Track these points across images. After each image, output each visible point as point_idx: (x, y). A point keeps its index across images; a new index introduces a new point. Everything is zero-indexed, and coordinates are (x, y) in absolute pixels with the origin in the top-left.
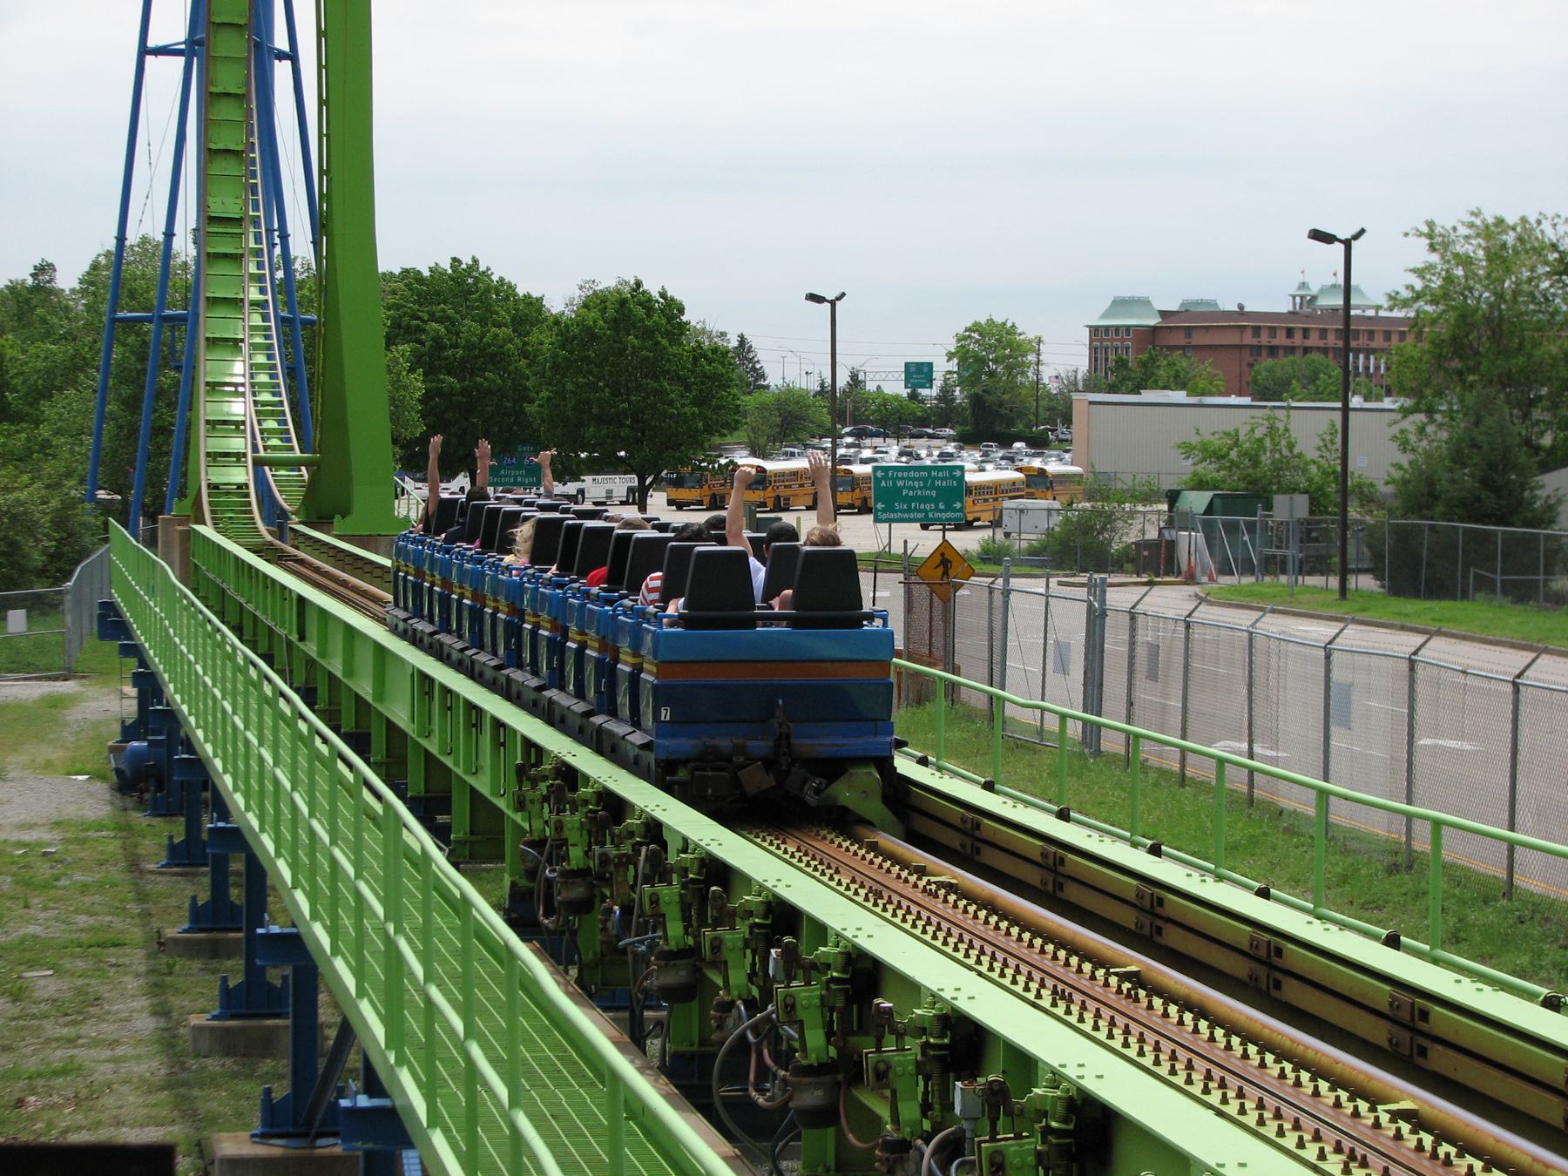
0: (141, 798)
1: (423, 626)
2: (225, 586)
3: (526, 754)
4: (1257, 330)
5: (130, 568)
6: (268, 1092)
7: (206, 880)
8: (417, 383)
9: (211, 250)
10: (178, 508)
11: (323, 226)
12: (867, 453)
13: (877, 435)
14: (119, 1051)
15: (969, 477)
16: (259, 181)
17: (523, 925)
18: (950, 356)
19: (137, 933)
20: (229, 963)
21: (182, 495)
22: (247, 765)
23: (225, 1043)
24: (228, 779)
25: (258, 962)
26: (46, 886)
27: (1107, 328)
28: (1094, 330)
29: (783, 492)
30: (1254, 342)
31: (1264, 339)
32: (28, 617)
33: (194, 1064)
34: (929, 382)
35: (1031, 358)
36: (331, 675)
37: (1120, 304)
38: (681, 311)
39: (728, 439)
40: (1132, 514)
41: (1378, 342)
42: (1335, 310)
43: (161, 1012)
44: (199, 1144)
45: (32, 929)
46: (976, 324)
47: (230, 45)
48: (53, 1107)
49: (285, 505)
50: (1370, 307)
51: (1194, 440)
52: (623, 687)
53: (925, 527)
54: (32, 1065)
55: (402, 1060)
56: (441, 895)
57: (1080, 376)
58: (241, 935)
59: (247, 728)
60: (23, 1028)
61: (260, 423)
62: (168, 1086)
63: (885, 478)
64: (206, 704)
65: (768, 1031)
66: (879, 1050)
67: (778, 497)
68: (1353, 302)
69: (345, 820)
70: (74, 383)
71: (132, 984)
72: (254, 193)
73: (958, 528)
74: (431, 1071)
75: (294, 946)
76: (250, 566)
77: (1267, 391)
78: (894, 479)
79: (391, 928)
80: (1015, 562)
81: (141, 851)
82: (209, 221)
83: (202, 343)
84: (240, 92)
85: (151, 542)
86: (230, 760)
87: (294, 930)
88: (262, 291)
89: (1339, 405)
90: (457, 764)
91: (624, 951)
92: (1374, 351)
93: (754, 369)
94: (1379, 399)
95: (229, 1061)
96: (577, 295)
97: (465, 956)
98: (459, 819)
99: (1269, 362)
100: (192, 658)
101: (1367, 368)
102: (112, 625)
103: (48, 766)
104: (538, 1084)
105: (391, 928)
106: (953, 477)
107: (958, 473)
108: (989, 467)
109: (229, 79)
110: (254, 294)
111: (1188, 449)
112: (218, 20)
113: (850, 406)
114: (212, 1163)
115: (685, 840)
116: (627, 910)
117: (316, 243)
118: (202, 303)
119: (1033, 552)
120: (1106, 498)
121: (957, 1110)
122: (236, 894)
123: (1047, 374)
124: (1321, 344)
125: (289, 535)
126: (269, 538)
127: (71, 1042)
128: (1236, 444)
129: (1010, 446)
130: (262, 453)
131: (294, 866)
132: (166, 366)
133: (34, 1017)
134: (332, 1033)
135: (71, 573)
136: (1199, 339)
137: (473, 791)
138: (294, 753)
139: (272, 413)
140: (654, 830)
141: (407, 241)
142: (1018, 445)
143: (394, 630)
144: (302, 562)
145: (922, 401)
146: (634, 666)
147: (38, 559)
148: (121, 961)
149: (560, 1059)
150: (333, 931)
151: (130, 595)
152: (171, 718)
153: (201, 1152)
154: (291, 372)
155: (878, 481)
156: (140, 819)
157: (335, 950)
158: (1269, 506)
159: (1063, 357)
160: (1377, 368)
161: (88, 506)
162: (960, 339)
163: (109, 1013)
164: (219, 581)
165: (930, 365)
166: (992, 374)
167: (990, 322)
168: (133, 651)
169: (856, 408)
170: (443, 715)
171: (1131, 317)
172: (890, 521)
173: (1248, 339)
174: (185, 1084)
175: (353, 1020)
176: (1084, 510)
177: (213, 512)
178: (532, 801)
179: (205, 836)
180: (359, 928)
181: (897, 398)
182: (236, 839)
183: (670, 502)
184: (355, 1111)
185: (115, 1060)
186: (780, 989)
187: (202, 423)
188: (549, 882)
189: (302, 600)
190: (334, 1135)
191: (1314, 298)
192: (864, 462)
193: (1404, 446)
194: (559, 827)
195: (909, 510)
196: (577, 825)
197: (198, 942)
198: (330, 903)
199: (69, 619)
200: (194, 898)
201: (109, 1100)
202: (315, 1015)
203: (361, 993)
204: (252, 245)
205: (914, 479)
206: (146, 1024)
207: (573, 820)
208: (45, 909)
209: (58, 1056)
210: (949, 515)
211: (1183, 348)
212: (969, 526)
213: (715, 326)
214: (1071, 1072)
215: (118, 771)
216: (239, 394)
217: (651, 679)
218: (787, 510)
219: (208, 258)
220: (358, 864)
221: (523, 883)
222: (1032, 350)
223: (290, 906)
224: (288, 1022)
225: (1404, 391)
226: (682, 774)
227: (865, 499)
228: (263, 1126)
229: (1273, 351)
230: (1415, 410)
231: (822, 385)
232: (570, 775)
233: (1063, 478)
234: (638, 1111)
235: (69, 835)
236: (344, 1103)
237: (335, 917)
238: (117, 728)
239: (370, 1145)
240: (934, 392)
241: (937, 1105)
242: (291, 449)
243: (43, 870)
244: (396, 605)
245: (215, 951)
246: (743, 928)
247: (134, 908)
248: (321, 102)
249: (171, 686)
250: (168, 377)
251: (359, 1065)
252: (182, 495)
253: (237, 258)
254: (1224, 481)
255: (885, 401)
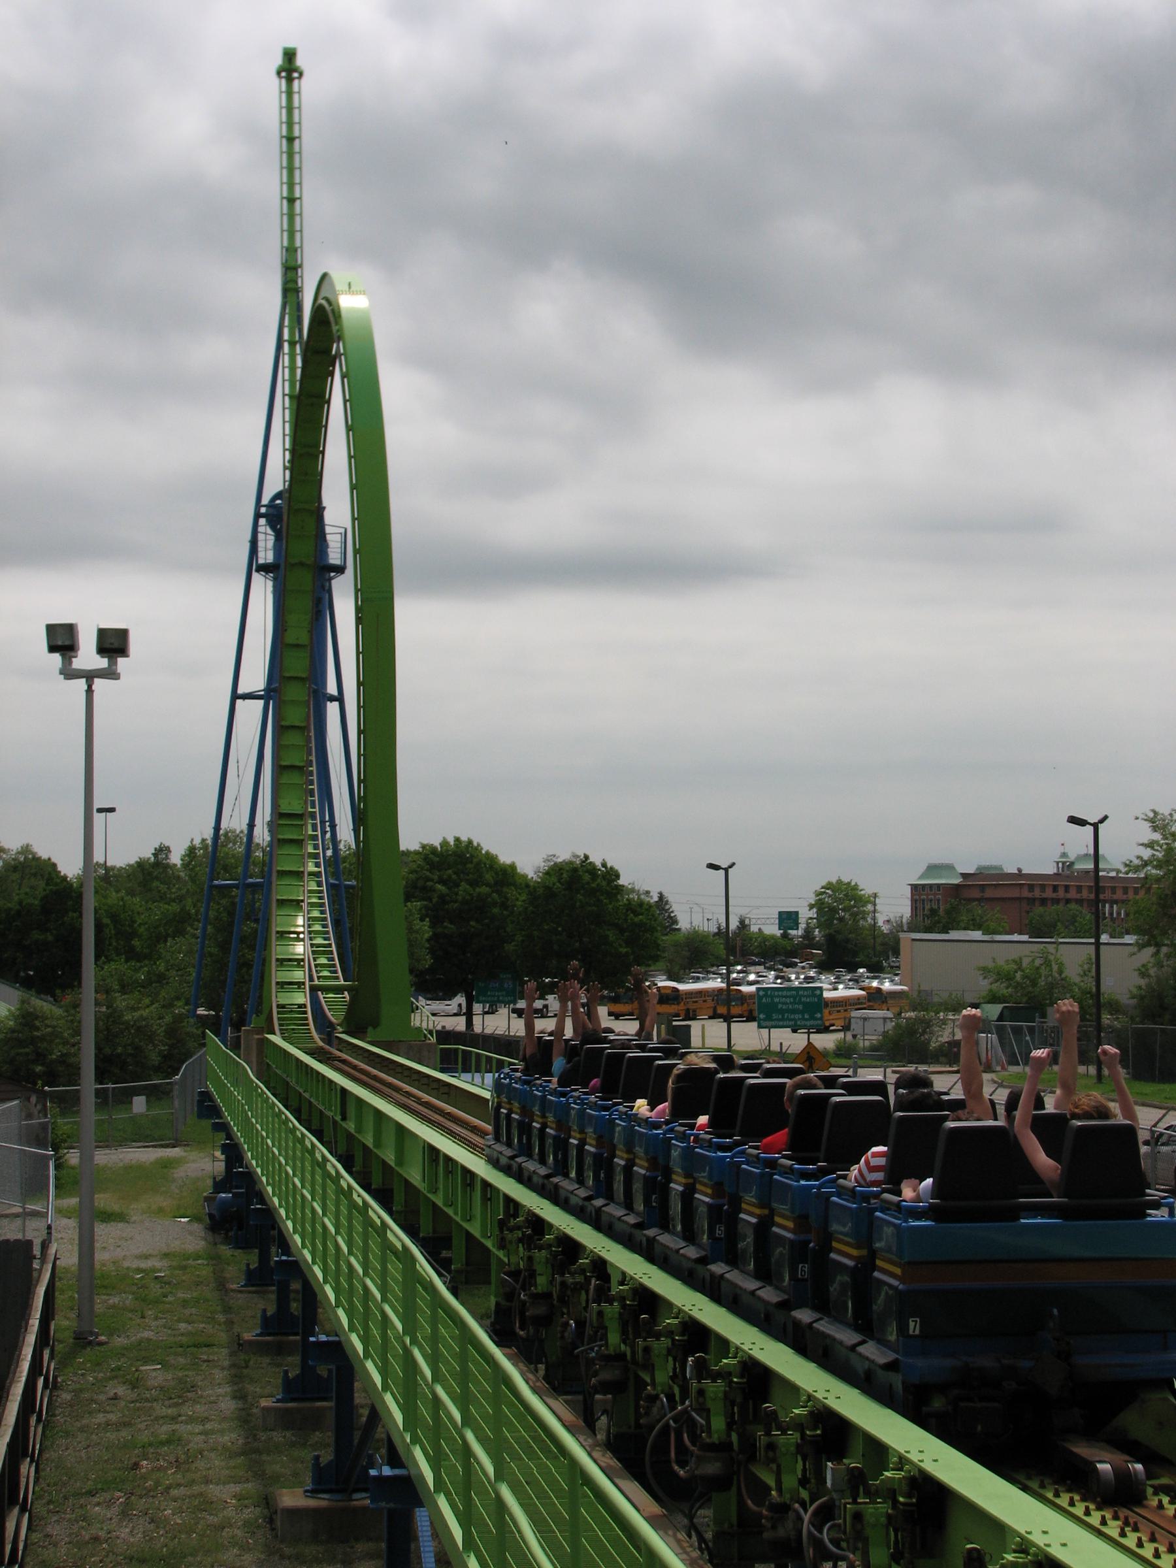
0: (226, 1234)
1: (531, 1166)
2: (288, 1079)
3: (507, 1207)
4: (1031, 887)
5: (222, 1067)
6: (317, 1458)
7: (273, 1297)
8: (425, 929)
9: (281, 837)
10: (255, 1022)
11: (361, 819)
12: (752, 977)
13: (759, 964)
14: (208, 1426)
15: (826, 995)
16: (315, 787)
17: (502, 1337)
18: (811, 907)
19: (223, 1337)
20: (290, 1359)
21: (258, 1012)
22: (303, 1213)
23: (285, 1420)
24: (290, 1224)
25: (310, 1362)
26: (157, 1302)
27: (924, 886)
28: (915, 888)
29: (692, 1006)
30: (1030, 895)
31: (1037, 893)
32: (147, 1102)
33: (263, 1436)
34: (796, 926)
35: (870, 907)
36: (384, 1163)
37: (933, 869)
38: (618, 876)
39: (652, 968)
40: (944, 1022)
41: (1119, 895)
42: (1087, 872)
43: (240, 1396)
44: (266, 1498)
45: (147, 1334)
46: (829, 883)
47: (295, 692)
48: (159, 1469)
49: (333, 1019)
50: (1113, 870)
51: (990, 965)
52: (619, 1178)
53: (794, 1031)
54: (144, 1437)
55: (415, 1440)
56: (444, 1311)
57: (904, 920)
58: (298, 1338)
59: (303, 1186)
60: (138, 1409)
61: (315, 960)
62: (243, 1453)
63: (766, 995)
64: (274, 1167)
65: (684, 1419)
66: (855, 1502)
67: (688, 1010)
68: (1101, 866)
69: (394, 1279)
70: (180, 932)
71: (219, 1375)
72: (312, 796)
73: (818, 1032)
74: (437, 1448)
75: (337, 1351)
76: (307, 1065)
77: (1038, 930)
78: (772, 997)
79: (408, 1340)
80: (861, 1057)
81: (228, 1275)
82: (280, 816)
83: (274, 904)
84: (303, 724)
85: (236, 1046)
86: (291, 1209)
87: (336, 1339)
88: (317, 865)
89: (1093, 940)
90: (456, 1214)
91: (577, 1356)
92: (1116, 902)
93: (669, 917)
94: (1121, 936)
95: (288, 1434)
96: (544, 866)
97: (463, 1358)
98: (457, 1254)
99: (1041, 909)
100: (264, 1134)
101: (1111, 914)
102: (207, 1108)
103: (161, 1210)
104: (516, 1457)
105: (408, 1340)
106: (814, 995)
107: (818, 992)
108: (841, 986)
109: (294, 716)
110: (311, 867)
111: (985, 971)
112: (287, 675)
113: (739, 943)
114: (276, 1512)
115: (624, 1274)
116: (581, 1324)
117: (356, 831)
118: (274, 875)
119: (873, 1048)
120: (926, 1010)
121: (829, 1483)
122: (295, 1307)
123: (881, 920)
124: (1078, 896)
125: (335, 1042)
126: (321, 1044)
127: (174, 1419)
128: (1020, 968)
129: (855, 971)
130: (316, 982)
131: (337, 1290)
132: (248, 919)
133: (147, 1400)
134: (365, 1412)
135: (179, 1069)
136: (989, 894)
137: (468, 1233)
138: (337, 1204)
139: (324, 953)
140: (600, 1266)
141: (420, 825)
142: (861, 970)
143: (494, 1163)
144: (344, 1061)
145: (791, 939)
146: (627, 1160)
147: (154, 1058)
148: (211, 1357)
149: (533, 1438)
150: (365, 1340)
151: (221, 1086)
152: (249, 1178)
153: (268, 1503)
154: (337, 923)
155: (760, 998)
156: (225, 1250)
157: (367, 1355)
158: (1044, 1015)
159: (892, 907)
160: (1119, 914)
161: (192, 1020)
162: (818, 894)
163: (202, 1397)
164: (284, 1076)
165: (797, 913)
166: (841, 919)
167: (839, 882)
168: (223, 1127)
169: (743, 945)
170: (464, 1192)
171: (941, 877)
172: (770, 1028)
173: (1026, 894)
174: (257, 1451)
175: (379, 1407)
176: (910, 1018)
177: (280, 1025)
178: (511, 1242)
179: (272, 1263)
180: (384, 1336)
181: (773, 937)
182: (296, 1269)
183: (610, 1014)
184: (380, 1479)
185: (205, 1433)
186: (694, 1384)
187: (274, 960)
188: (524, 1303)
189: (344, 1091)
190: (365, 1490)
191: (1072, 863)
192: (751, 983)
193: (1143, 973)
194: (530, 1259)
195: (783, 1019)
196: (543, 1260)
197: (267, 1343)
198: (364, 1316)
199: (176, 1103)
200: (264, 1311)
201: (200, 1464)
202: (352, 1398)
203: (386, 1387)
204: (310, 832)
205: (786, 997)
206: (228, 1405)
207: (541, 1256)
208: (156, 1318)
209: (164, 1430)
210: (812, 1022)
211: (977, 900)
212: (825, 1030)
213: (642, 886)
214: (914, 1457)
215: (211, 1216)
216: (301, 938)
217: (643, 1172)
218: (694, 1019)
219: (278, 842)
220: (383, 1289)
221: (503, 1303)
222: (869, 902)
223: (332, 1317)
224: (331, 1404)
225: (1138, 931)
226: (938, 1403)
227: (751, 1011)
228: (313, 1482)
229: (1043, 901)
230: (1148, 944)
231: (719, 928)
232: (539, 1225)
233: (893, 995)
234: (588, 1480)
235: (174, 1263)
236: (373, 1472)
237: (366, 1329)
238: (210, 1182)
239: (392, 1505)
240: (800, 932)
241: (813, 1479)
242: (337, 978)
243: (156, 1290)
244: (497, 1138)
245: (279, 1350)
246: (665, 1342)
247: (221, 1318)
248: (360, 732)
249: (249, 1154)
250: (248, 927)
251: (384, 1436)
252: (258, 1012)
253: (299, 843)
254: (1011, 996)
255: (763, 938)
